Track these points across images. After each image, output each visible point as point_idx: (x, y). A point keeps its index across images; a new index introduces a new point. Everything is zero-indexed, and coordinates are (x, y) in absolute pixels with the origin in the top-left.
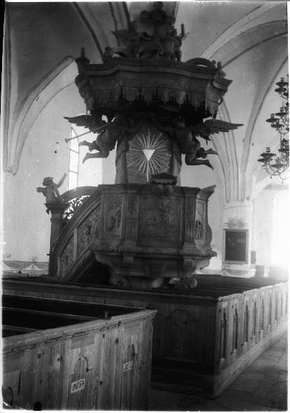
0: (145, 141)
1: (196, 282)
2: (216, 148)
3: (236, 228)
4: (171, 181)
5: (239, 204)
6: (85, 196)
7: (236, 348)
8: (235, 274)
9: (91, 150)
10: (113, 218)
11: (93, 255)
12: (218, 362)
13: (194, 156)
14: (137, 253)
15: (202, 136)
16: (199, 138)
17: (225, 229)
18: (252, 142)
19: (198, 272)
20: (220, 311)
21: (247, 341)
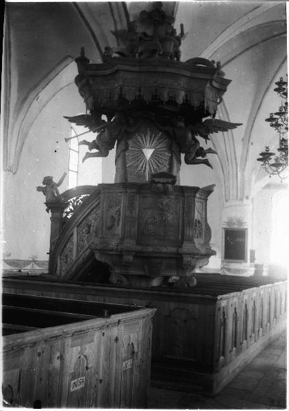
0: (144, 140)
1: (195, 280)
2: (215, 148)
3: (236, 227)
4: (170, 180)
5: (238, 203)
6: (85, 196)
7: (235, 346)
8: (234, 273)
9: (90, 149)
10: (113, 217)
11: (92, 254)
12: (218, 360)
13: (194, 155)
14: (137, 252)
15: (202, 135)
16: (198, 138)
17: (224, 228)
18: (251, 141)
19: (197, 271)
20: (219, 310)
21: (246, 339)
